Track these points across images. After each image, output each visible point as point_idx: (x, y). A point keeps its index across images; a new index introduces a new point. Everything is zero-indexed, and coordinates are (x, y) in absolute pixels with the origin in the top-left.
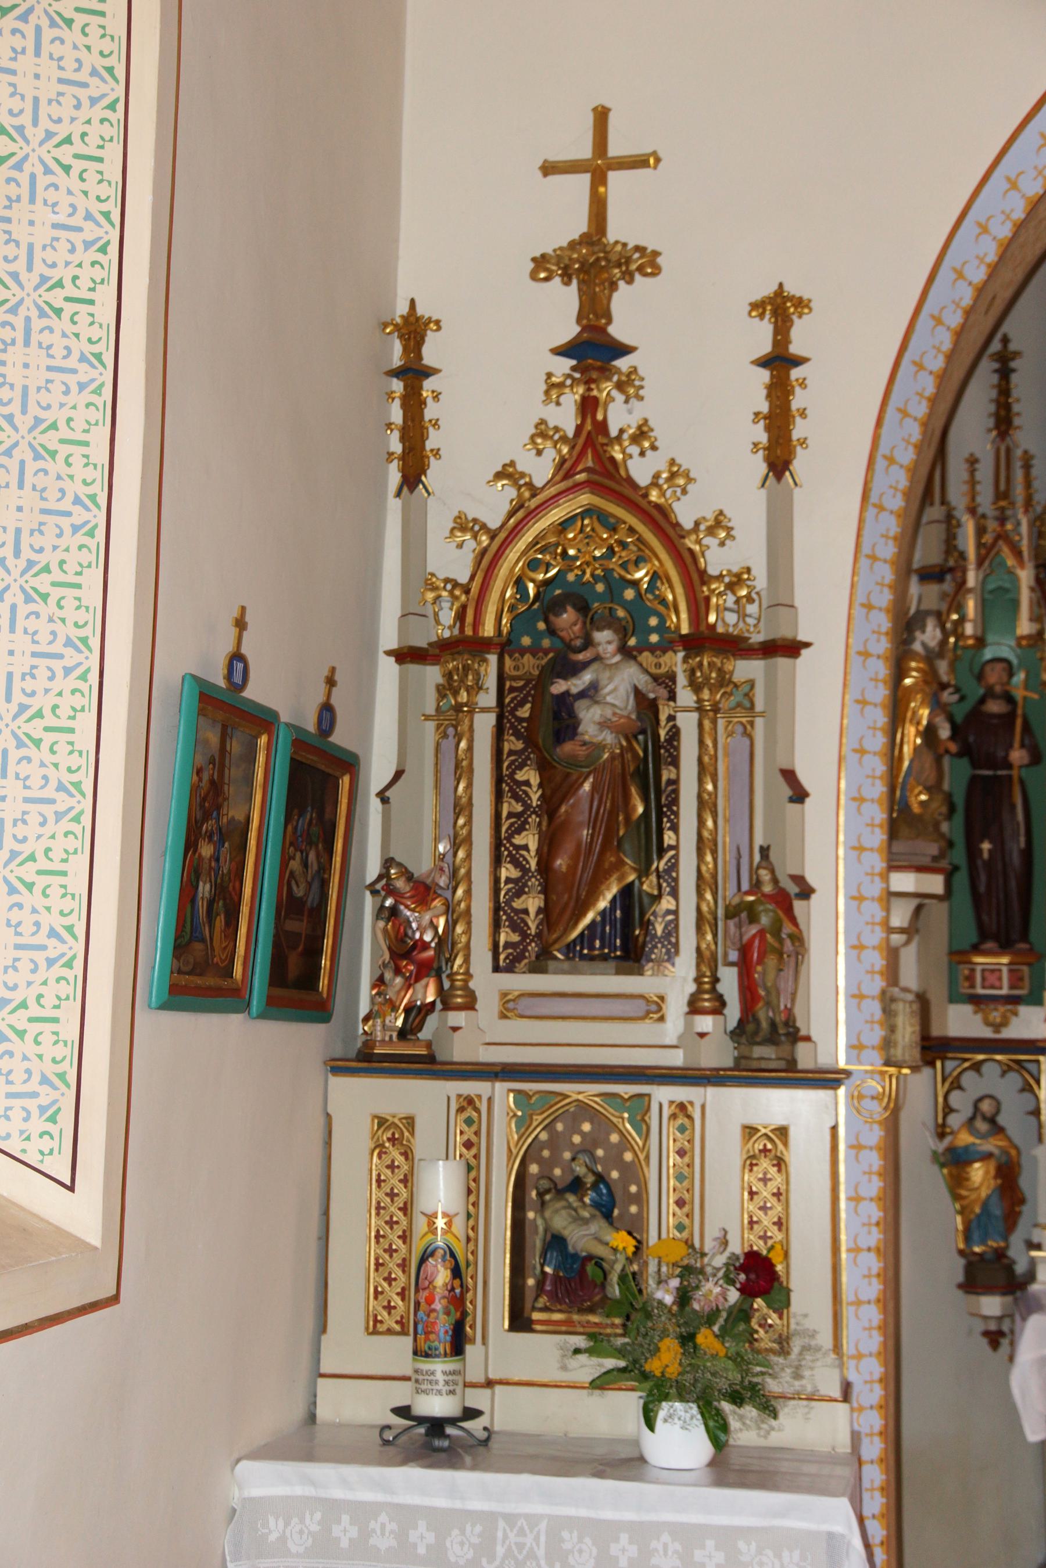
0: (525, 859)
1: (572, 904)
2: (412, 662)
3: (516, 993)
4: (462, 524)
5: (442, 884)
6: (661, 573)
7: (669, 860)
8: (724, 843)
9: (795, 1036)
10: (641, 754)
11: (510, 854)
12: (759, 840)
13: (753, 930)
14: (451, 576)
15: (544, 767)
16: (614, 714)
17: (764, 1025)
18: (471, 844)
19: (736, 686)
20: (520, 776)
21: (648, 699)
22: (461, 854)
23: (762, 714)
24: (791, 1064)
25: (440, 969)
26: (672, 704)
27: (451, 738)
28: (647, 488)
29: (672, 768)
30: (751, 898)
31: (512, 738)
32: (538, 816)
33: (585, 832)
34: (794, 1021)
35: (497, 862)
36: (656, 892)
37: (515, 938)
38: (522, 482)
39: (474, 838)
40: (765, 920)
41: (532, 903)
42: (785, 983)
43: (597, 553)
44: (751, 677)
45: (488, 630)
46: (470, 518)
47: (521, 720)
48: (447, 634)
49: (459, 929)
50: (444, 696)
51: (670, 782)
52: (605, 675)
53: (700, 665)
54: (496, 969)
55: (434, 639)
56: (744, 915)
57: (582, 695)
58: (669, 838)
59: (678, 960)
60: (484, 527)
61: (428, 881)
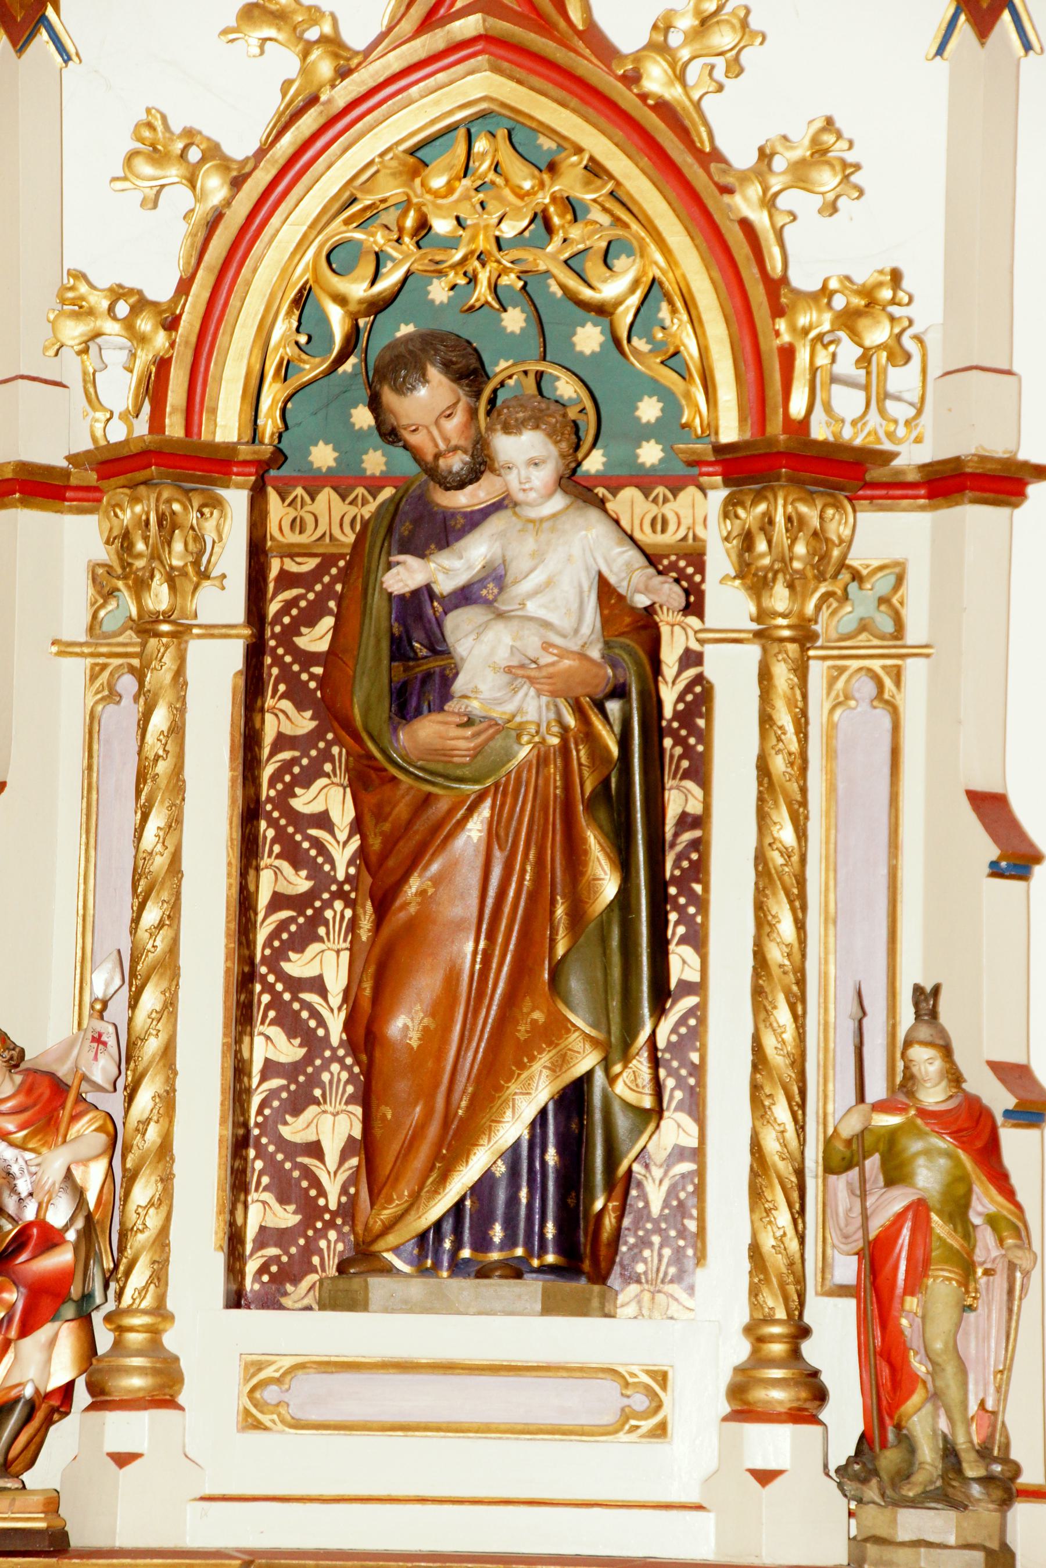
0: (315, 1014)
1: (433, 1130)
2: (24, 503)
3: (287, 1363)
4: (158, 145)
5: (98, 1077)
6: (670, 286)
7: (682, 1021)
8: (824, 976)
10: (615, 750)
11: (276, 1001)
12: (912, 973)
13: (897, 1200)
14: (129, 284)
15: (366, 779)
16: (547, 646)
17: (928, 1453)
18: (175, 975)
19: (857, 576)
20: (304, 802)
21: (633, 609)
22: (151, 999)
23: (922, 651)
25: (87, 1297)
26: (693, 621)
27: (127, 701)
28: (637, 57)
29: (689, 784)
30: (891, 1120)
31: (286, 705)
32: (350, 903)
33: (469, 947)
34: (1006, 1446)
35: (242, 1017)
36: (647, 1102)
37: (286, 1217)
38: (312, 34)
39: (183, 961)
40: (927, 1179)
41: (333, 1125)
43: (509, 230)
44: (897, 555)
45: (225, 426)
46: (177, 128)
47: (308, 659)
48: (117, 433)
49: (142, 1192)
50: (110, 594)
51: (687, 822)
52: (521, 551)
53: (767, 523)
54: (236, 1300)
55: (86, 445)
56: (873, 1164)
57: (465, 596)
58: (682, 964)
59: (701, 1277)
60: (213, 152)
61: (63, 1071)
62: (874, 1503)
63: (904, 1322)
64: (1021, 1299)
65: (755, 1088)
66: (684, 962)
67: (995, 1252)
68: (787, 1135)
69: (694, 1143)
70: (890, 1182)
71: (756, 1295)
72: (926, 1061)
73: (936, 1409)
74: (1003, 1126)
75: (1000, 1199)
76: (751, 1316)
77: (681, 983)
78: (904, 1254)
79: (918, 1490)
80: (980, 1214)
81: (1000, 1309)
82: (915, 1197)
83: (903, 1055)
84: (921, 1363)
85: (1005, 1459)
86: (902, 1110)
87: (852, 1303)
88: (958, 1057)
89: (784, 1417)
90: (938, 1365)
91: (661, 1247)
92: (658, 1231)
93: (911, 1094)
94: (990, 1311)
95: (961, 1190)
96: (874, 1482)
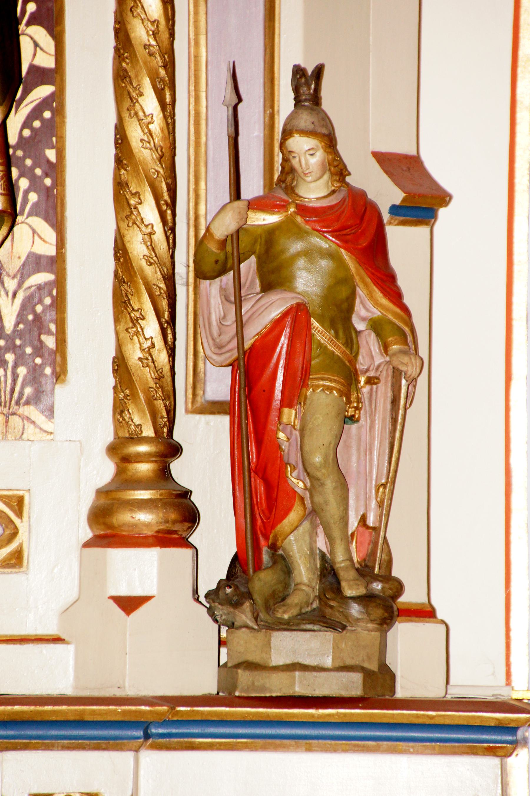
9: (388, 607)
12: (292, 53)
13: (276, 306)
17: (304, 573)
24: (379, 686)
30: (270, 219)
40: (308, 281)
42: (362, 452)
56: (249, 267)
58: (34, 46)
59: (62, 396)
62: (247, 627)
63: (281, 435)
64: (406, 409)
65: (120, 186)
66: (36, 45)
67: (379, 359)
68: (155, 237)
69: (52, 251)
70: (267, 287)
71: (122, 412)
72: (306, 151)
73: (314, 527)
74: (390, 223)
75: (385, 301)
76: (116, 433)
77: (33, 68)
78: (282, 363)
79: (294, 611)
80: (363, 319)
81: (384, 420)
82: (294, 302)
83: (282, 145)
84: (298, 478)
85: (387, 577)
86: (283, 207)
87: (225, 420)
88: (340, 147)
89: (151, 540)
90: (318, 479)
91: (16, 366)
92: (12, 348)
93: (290, 190)
94: (373, 422)
95: (344, 293)
96: (247, 605)
